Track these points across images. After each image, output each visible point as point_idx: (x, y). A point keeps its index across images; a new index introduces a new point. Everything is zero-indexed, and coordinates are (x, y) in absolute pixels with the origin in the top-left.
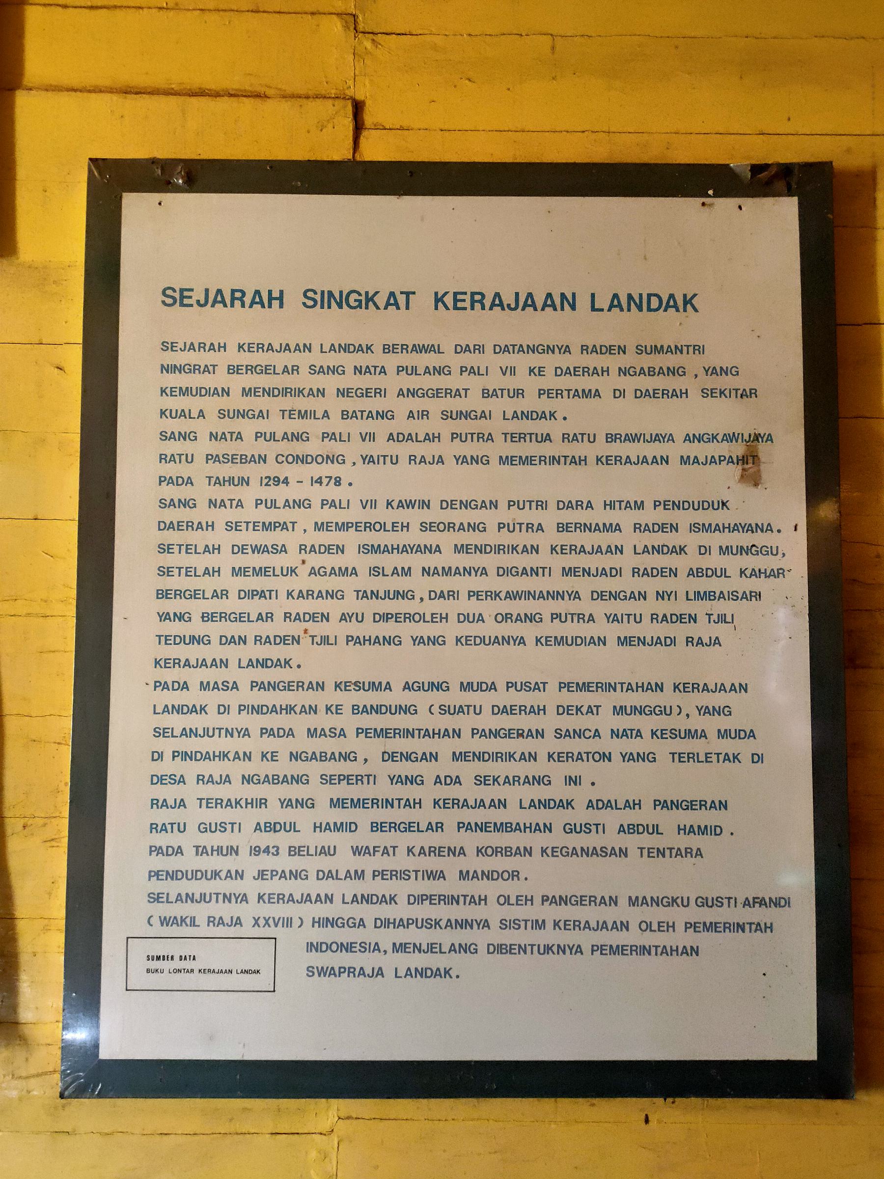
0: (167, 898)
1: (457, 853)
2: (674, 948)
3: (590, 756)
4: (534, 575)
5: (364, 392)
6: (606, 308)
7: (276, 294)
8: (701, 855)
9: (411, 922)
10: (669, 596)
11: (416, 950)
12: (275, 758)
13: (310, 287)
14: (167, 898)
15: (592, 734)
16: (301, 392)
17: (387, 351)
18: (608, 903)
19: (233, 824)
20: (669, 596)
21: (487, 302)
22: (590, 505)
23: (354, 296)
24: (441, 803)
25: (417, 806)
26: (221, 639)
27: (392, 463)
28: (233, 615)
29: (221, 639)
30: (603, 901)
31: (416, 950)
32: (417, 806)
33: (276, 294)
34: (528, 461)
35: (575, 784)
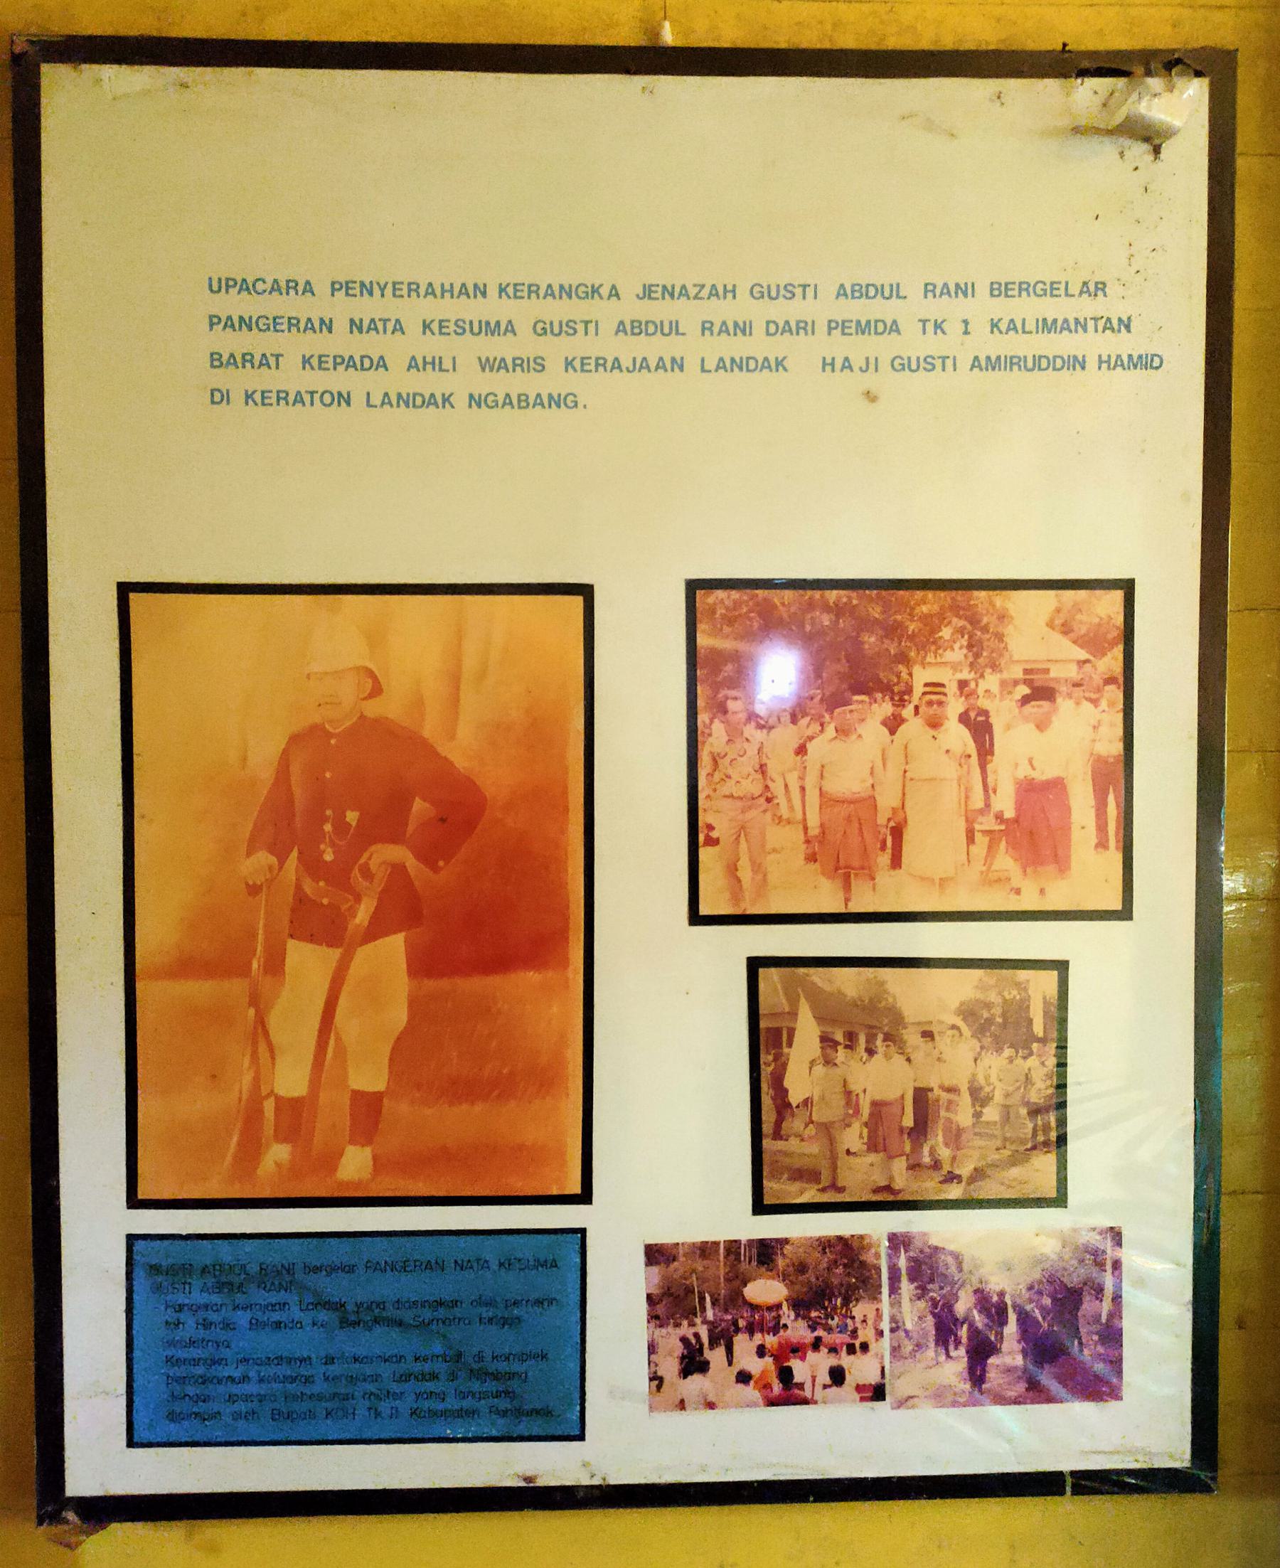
0: (1066, 289)
1: (676, 295)
2: (447, 287)
3: (317, 396)
4: (960, 294)
5: (1048, 287)
6: (1077, 293)
7: (730, 288)
8: (617, 295)
9: (337, 286)
10: (382, 290)
11: (667, 295)
12: (444, 330)
13: (748, 292)
14: (1066, 289)
15: (268, 286)
16: (595, 291)
17: (996, 293)
18: (546, 404)
19: (805, 287)
20: (382, 290)
21: (422, 291)
22: (309, 288)
23: (582, 289)
24: (510, 290)
25: (730, 295)
26: (212, 395)
27: (212, 291)
28: (1040, 286)
29: (212, 395)
30: (464, 290)
31: (667, 295)
32: (730, 295)
33: (730, 288)
34: (567, 292)
35: (965, 295)
